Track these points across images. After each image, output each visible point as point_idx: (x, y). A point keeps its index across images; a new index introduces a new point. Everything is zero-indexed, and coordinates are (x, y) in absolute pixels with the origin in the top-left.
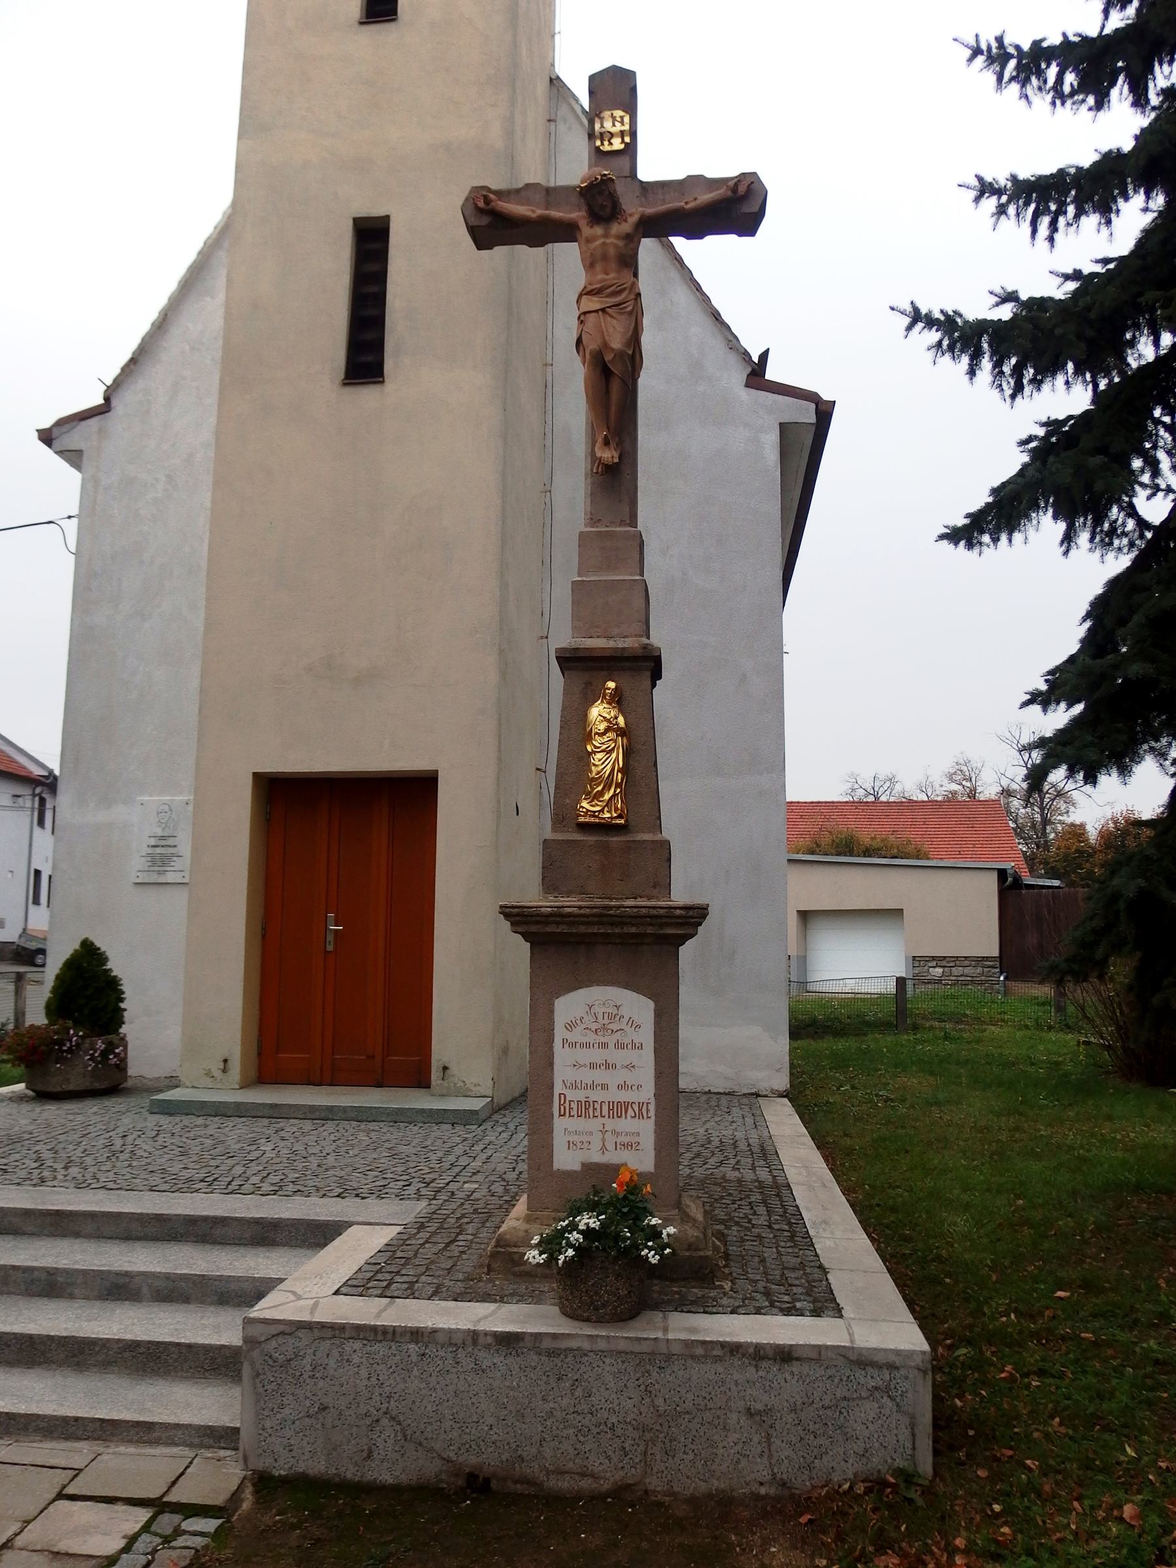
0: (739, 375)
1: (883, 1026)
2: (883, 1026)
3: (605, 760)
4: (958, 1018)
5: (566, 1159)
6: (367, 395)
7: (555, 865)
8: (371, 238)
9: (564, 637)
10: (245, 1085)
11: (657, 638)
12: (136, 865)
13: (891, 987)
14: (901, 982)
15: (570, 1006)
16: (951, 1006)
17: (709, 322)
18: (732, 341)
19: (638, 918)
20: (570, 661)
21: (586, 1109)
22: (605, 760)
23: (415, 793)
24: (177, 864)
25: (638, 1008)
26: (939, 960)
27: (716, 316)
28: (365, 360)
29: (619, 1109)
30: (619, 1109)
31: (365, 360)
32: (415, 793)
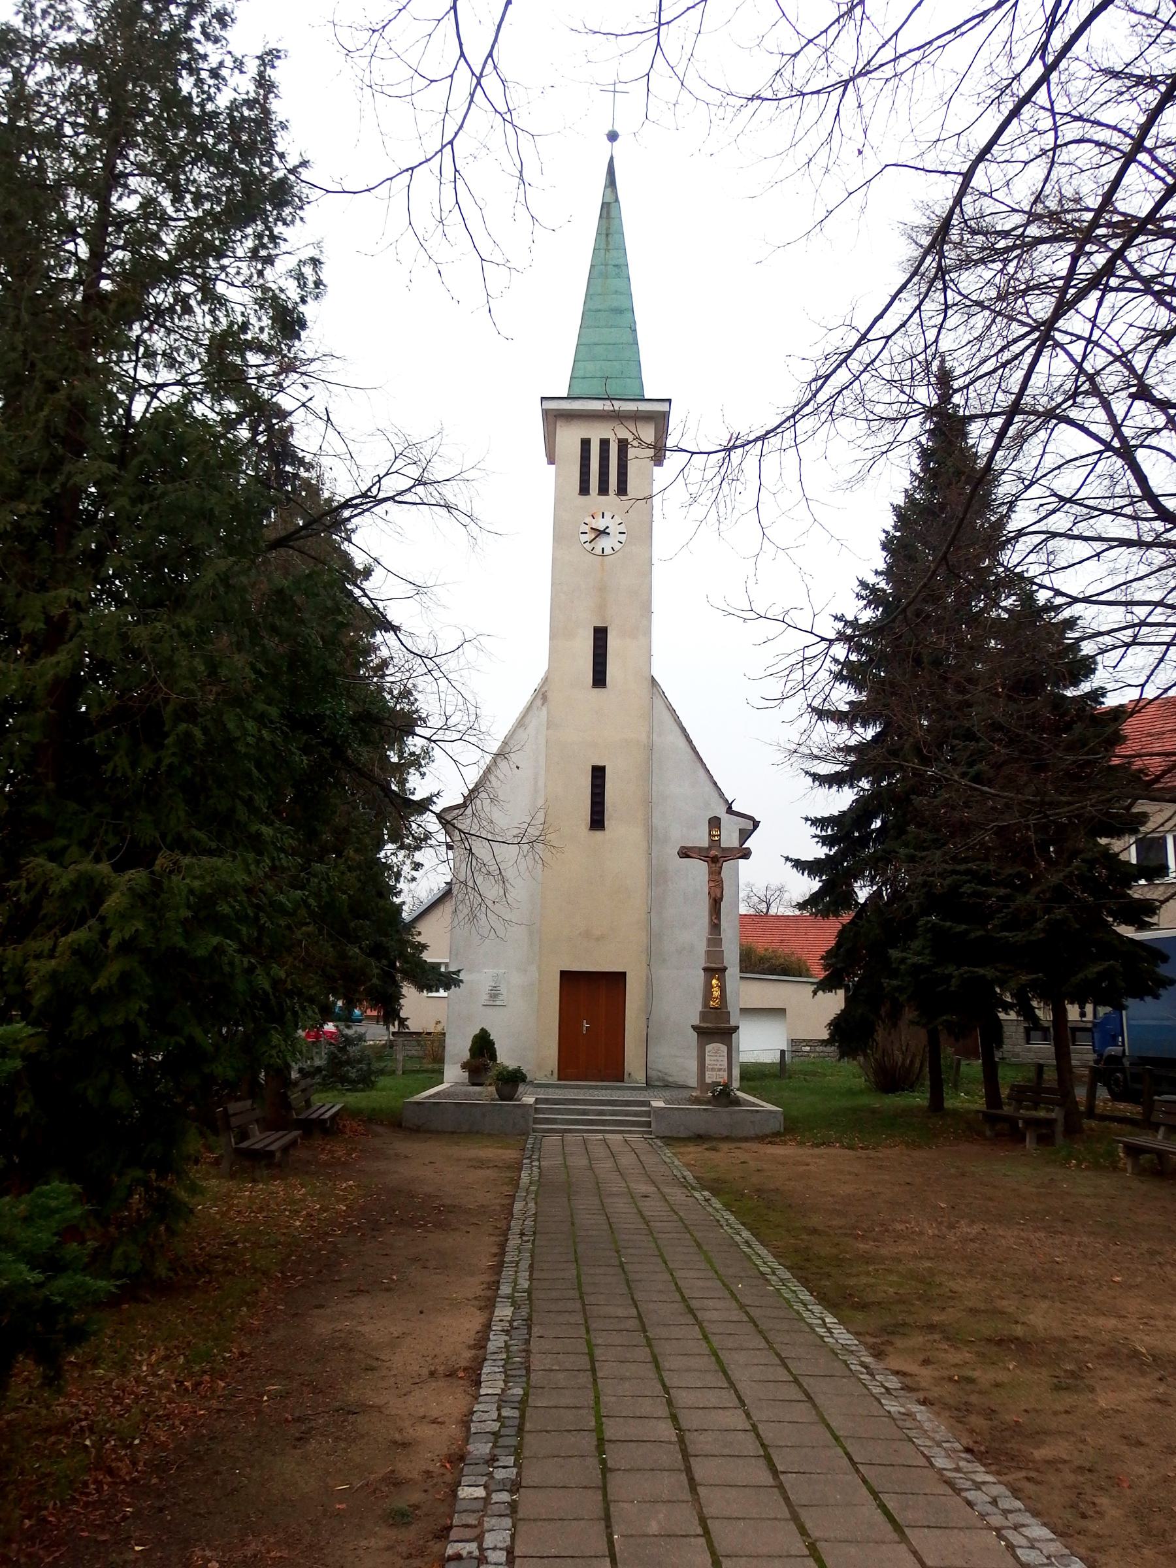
0: (725, 808)
1: (775, 1076)
2: (775, 1076)
3: (716, 993)
4: (814, 1074)
5: (708, 1081)
6: (598, 834)
7: (704, 1016)
8: (598, 773)
9: (704, 965)
10: (559, 1079)
11: (725, 964)
12: (484, 998)
13: (776, 1058)
14: (783, 1052)
15: (709, 1048)
16: (811, 1068)
17: (711, 785)
18: (721, 794)
19: (724, 1028)
20: (705, 969)
21: (712, 1070)
22: (716, 993)
23: (619, 978)
24: (501, 997)
25: (724, 1048)
26: (808, 1042)
27: (715, 784)
28: (597, 821)
29: (720, 1070)
30: (720, 1070)
31: (597, 821)
32: (619, 978)
